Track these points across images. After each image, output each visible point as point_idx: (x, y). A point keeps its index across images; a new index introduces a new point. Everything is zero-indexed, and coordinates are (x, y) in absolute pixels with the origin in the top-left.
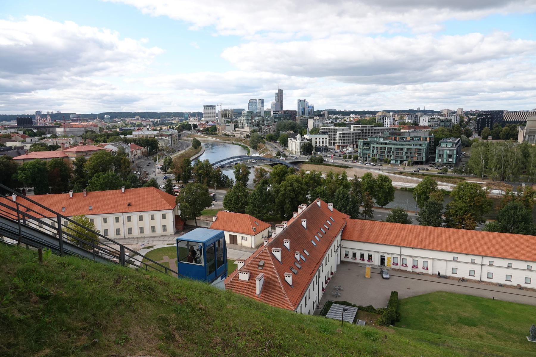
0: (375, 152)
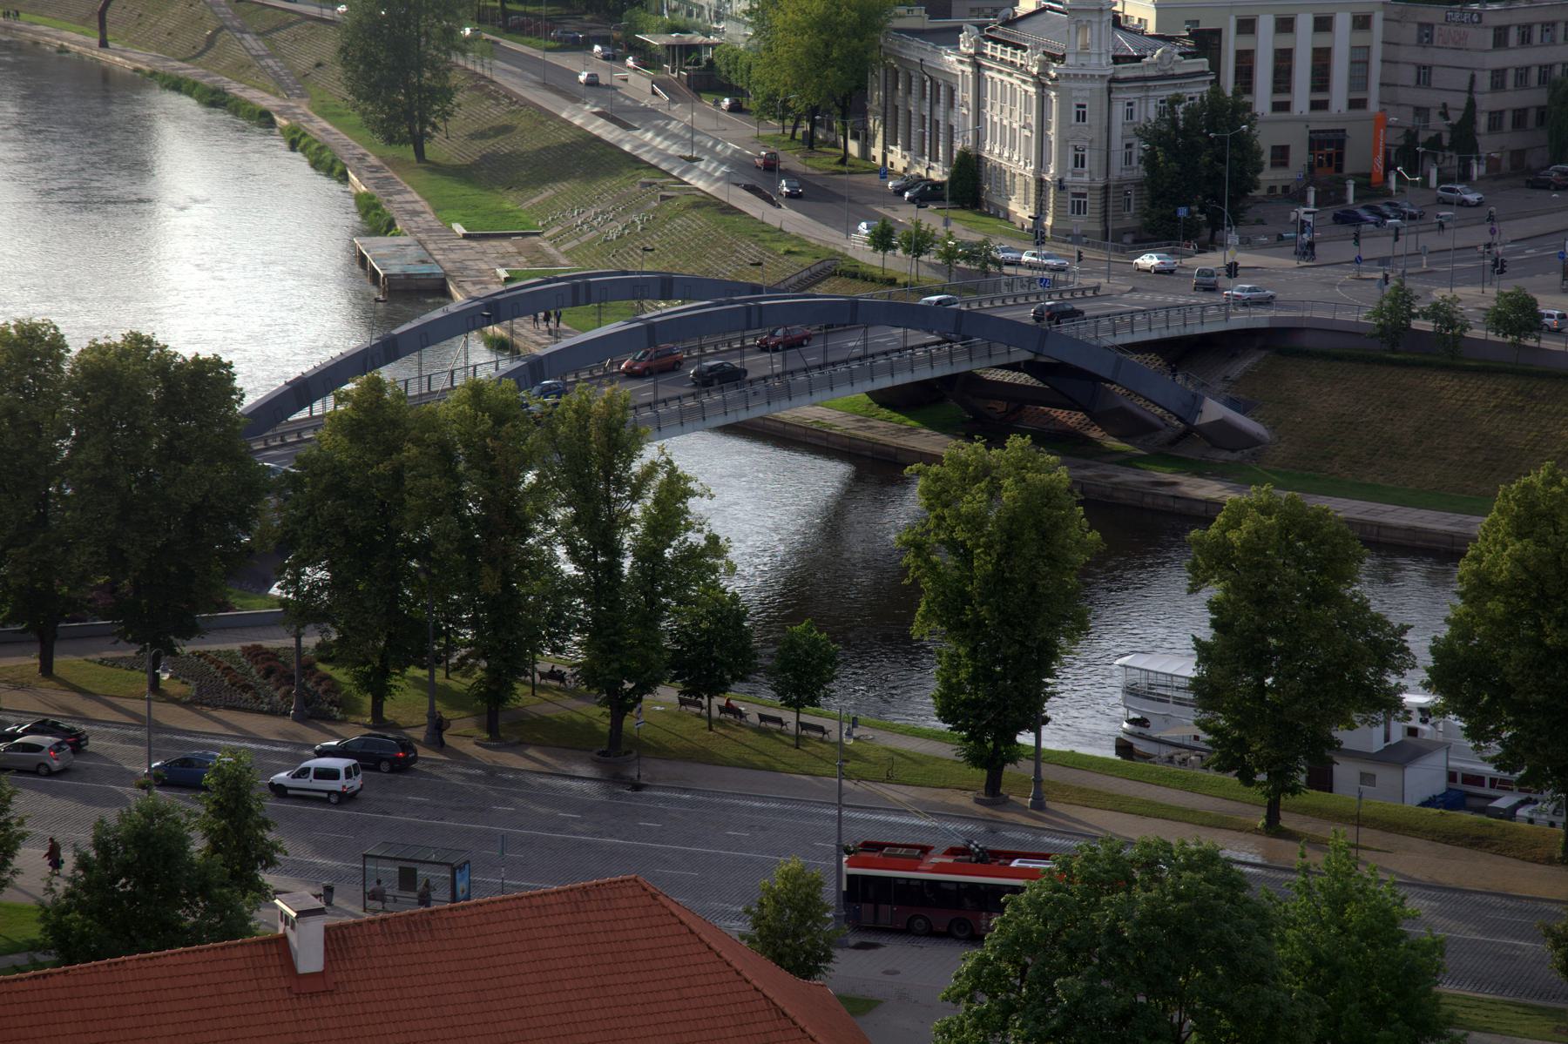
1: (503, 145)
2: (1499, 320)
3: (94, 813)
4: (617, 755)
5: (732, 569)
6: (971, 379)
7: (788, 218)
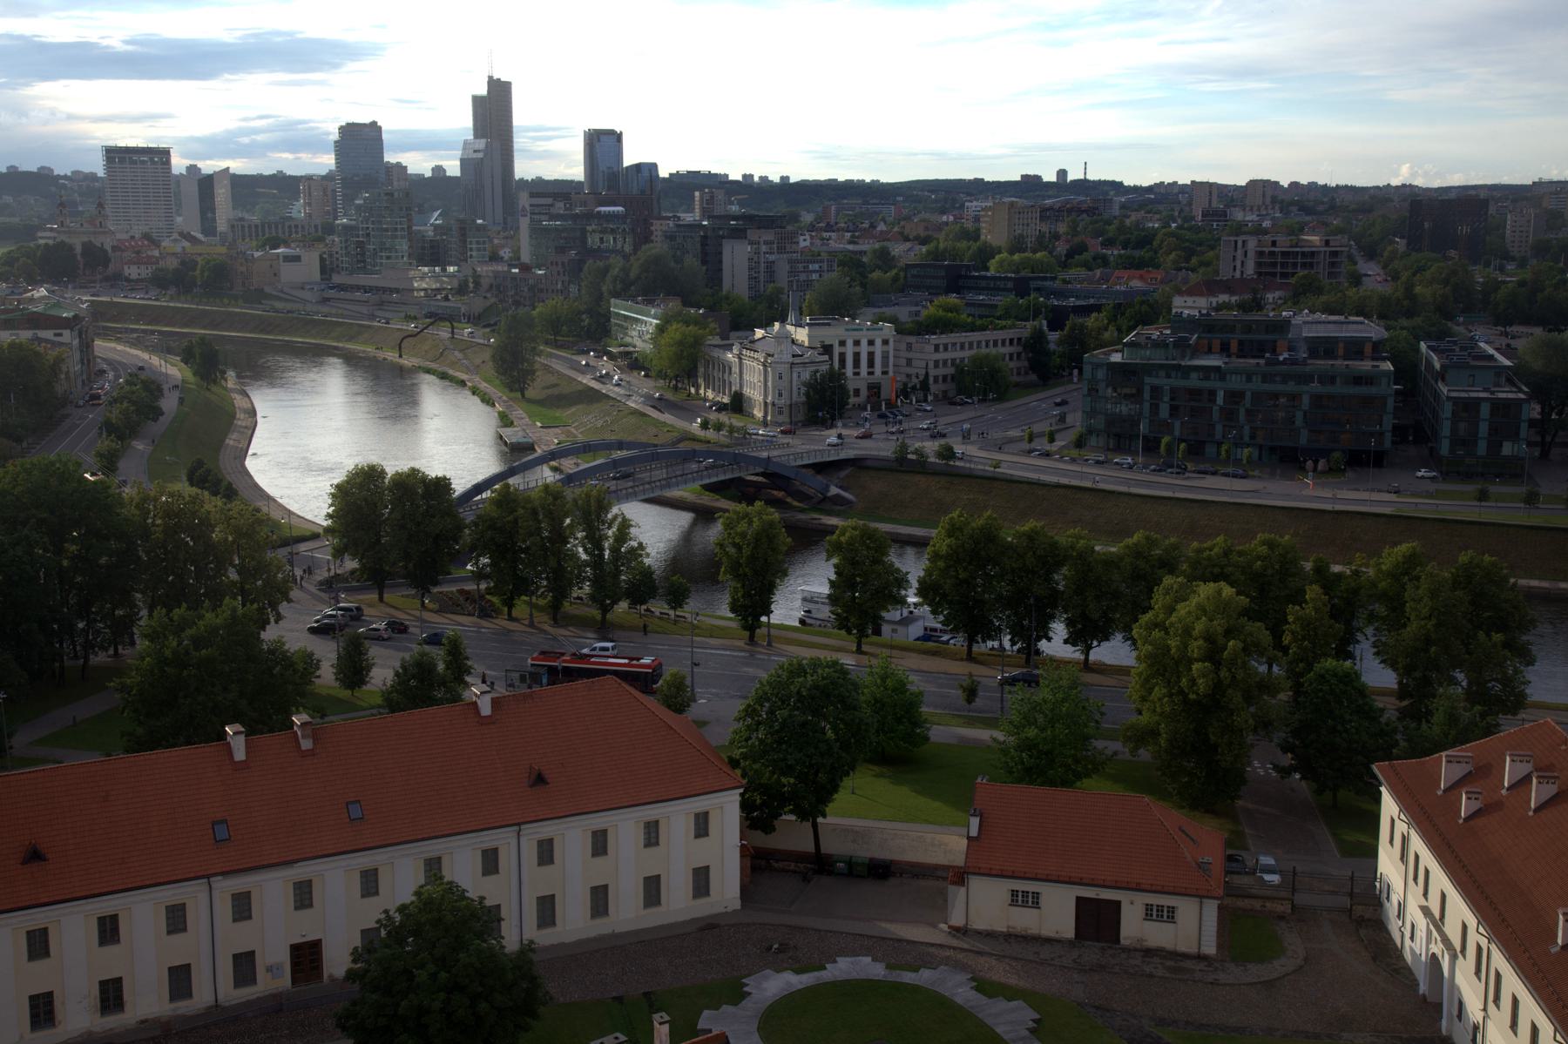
0: (1164, 411)
1: (555, 391)
2: (940, 455)
3: (401, 654)
5: (648, 555)
6: (740, 479)
7: (667, 418)
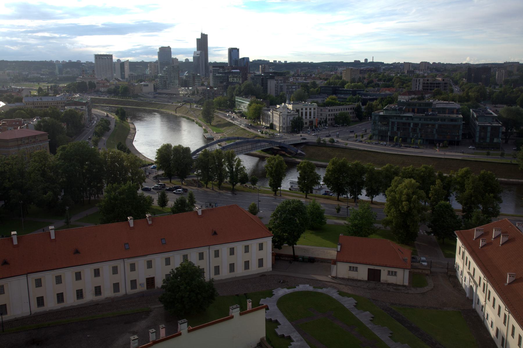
0: (395, 129)
1: (220, 123)
2: (330, 141)
4: (233, 191)
7: (251, 130)
